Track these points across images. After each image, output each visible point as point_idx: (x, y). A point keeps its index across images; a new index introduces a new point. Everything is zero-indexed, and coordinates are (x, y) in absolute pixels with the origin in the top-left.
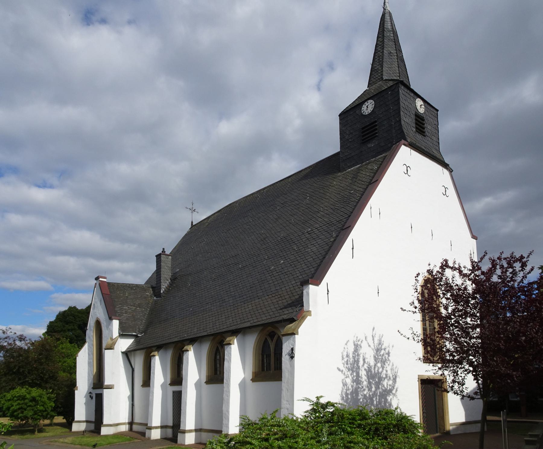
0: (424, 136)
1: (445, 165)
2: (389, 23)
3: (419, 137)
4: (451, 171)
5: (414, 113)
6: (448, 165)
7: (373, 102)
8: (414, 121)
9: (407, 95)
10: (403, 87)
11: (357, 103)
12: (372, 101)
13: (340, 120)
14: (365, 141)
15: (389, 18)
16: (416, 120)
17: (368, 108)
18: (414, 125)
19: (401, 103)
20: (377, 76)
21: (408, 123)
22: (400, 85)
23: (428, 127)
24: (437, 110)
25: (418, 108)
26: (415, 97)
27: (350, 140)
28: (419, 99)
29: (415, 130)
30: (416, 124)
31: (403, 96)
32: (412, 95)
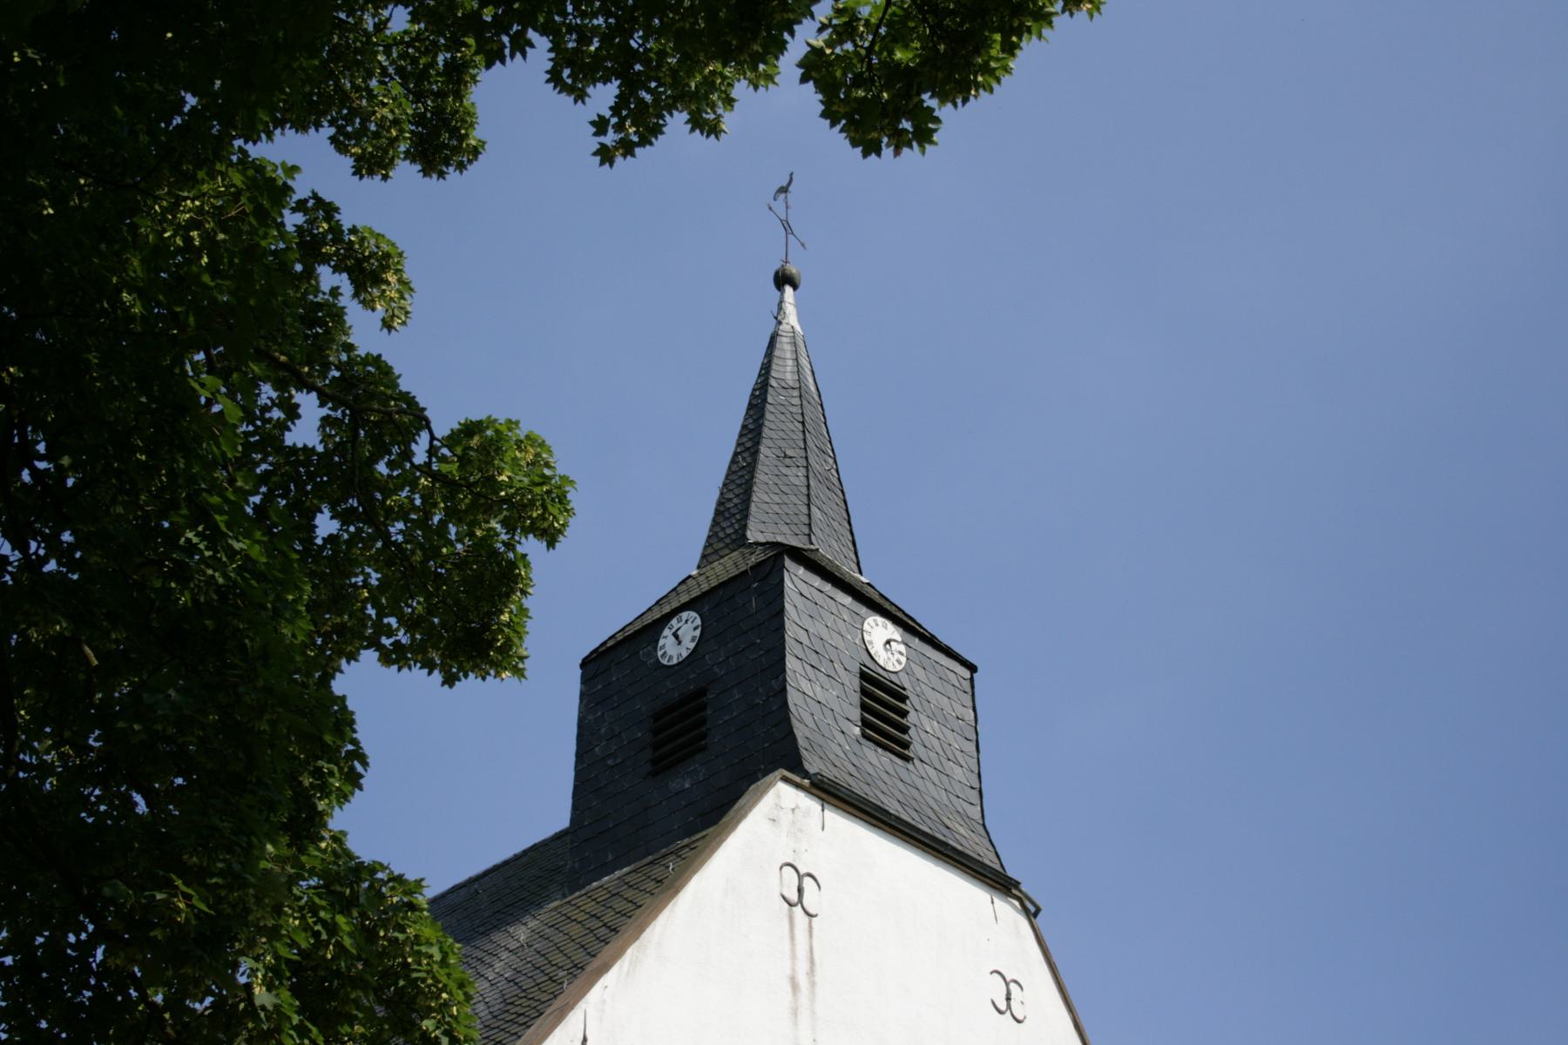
0: (907, 759)
1: (1000, 883)
2: (790, 363)
3: (877, 759)
4: (1031, 913)
5: (856, 668)
6: (1017, 884)
7: (698, 622)
8: (856, 698)
9: (818, 597)
10: (801, 571)
11: (649, 619)
12: (693, 614)
13: (586, 680)
14: (662, 766)
15: (788, 347)
16: (864, 692)
17: (678, 643)
18: (856, 714)
19: (788, 624)
20: (729, 531)
21: (819, 701)
22: (788, 563)
23: (921, 725)
24: (972, 668)
25: (877, 649)
26: (863, 610)
27: (610, 762)
28: (880, 620)
29: (857, 731)
30: (864, 707)
31: (798, 600)
32: (847, 600)
